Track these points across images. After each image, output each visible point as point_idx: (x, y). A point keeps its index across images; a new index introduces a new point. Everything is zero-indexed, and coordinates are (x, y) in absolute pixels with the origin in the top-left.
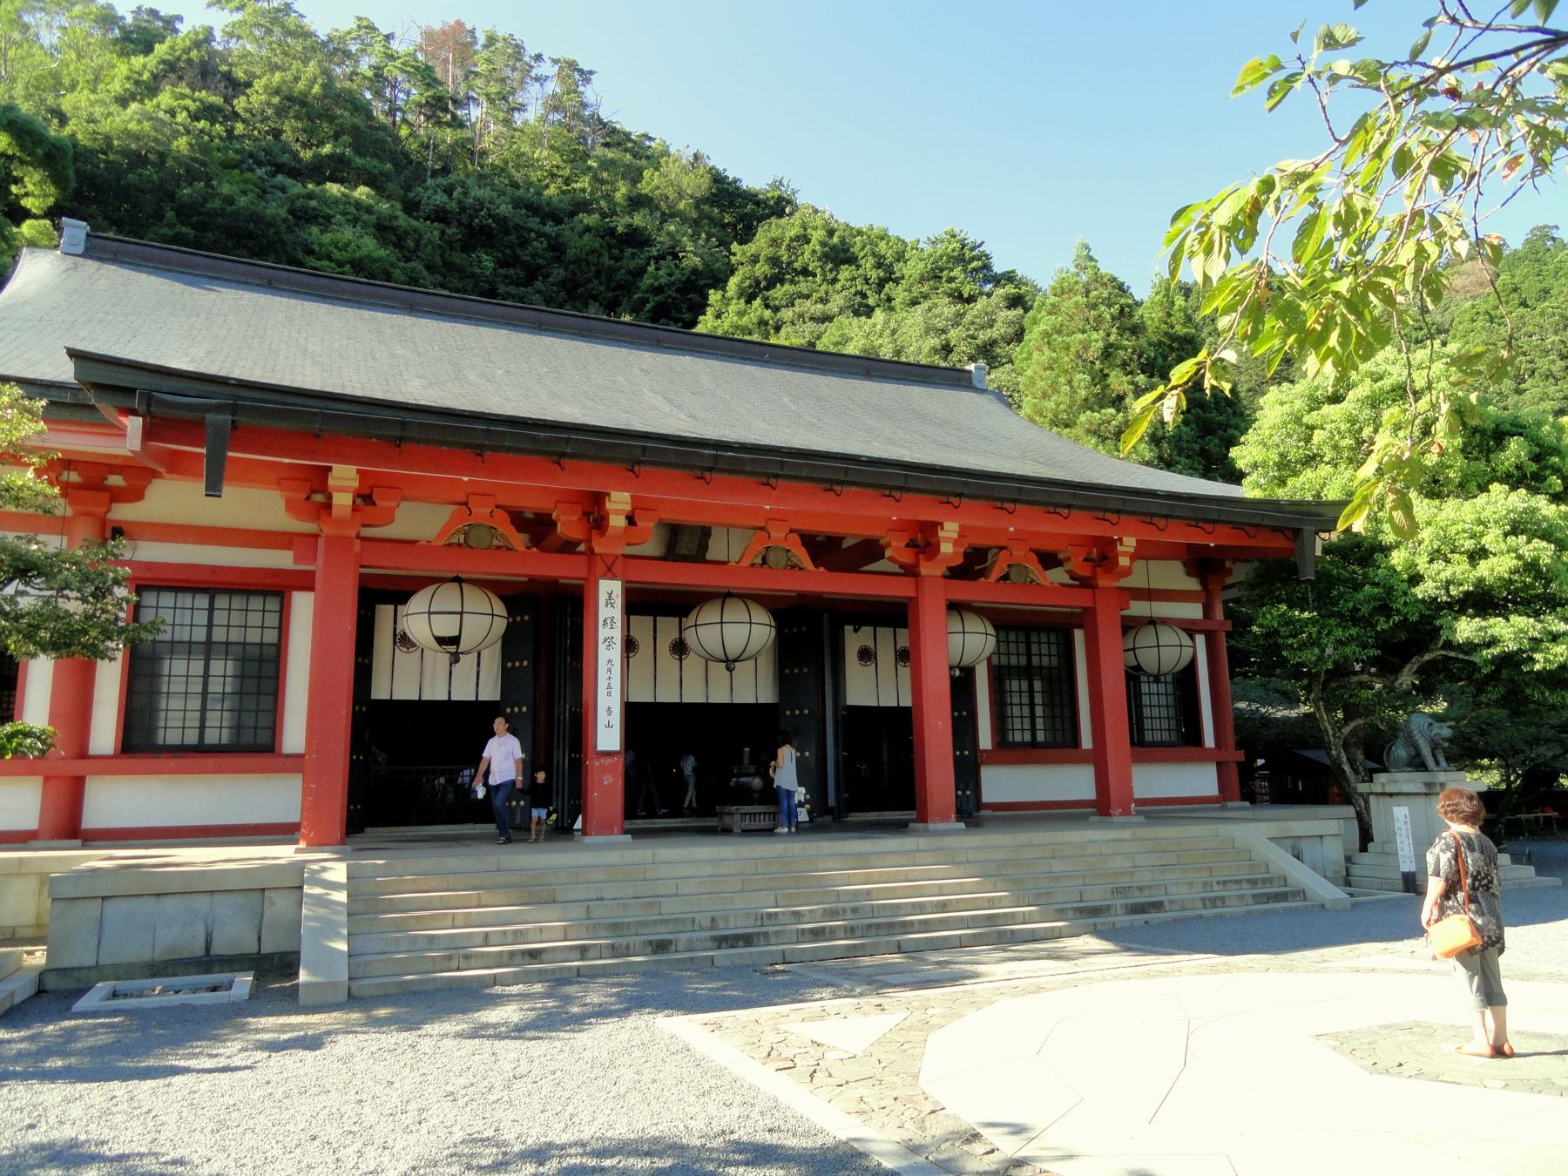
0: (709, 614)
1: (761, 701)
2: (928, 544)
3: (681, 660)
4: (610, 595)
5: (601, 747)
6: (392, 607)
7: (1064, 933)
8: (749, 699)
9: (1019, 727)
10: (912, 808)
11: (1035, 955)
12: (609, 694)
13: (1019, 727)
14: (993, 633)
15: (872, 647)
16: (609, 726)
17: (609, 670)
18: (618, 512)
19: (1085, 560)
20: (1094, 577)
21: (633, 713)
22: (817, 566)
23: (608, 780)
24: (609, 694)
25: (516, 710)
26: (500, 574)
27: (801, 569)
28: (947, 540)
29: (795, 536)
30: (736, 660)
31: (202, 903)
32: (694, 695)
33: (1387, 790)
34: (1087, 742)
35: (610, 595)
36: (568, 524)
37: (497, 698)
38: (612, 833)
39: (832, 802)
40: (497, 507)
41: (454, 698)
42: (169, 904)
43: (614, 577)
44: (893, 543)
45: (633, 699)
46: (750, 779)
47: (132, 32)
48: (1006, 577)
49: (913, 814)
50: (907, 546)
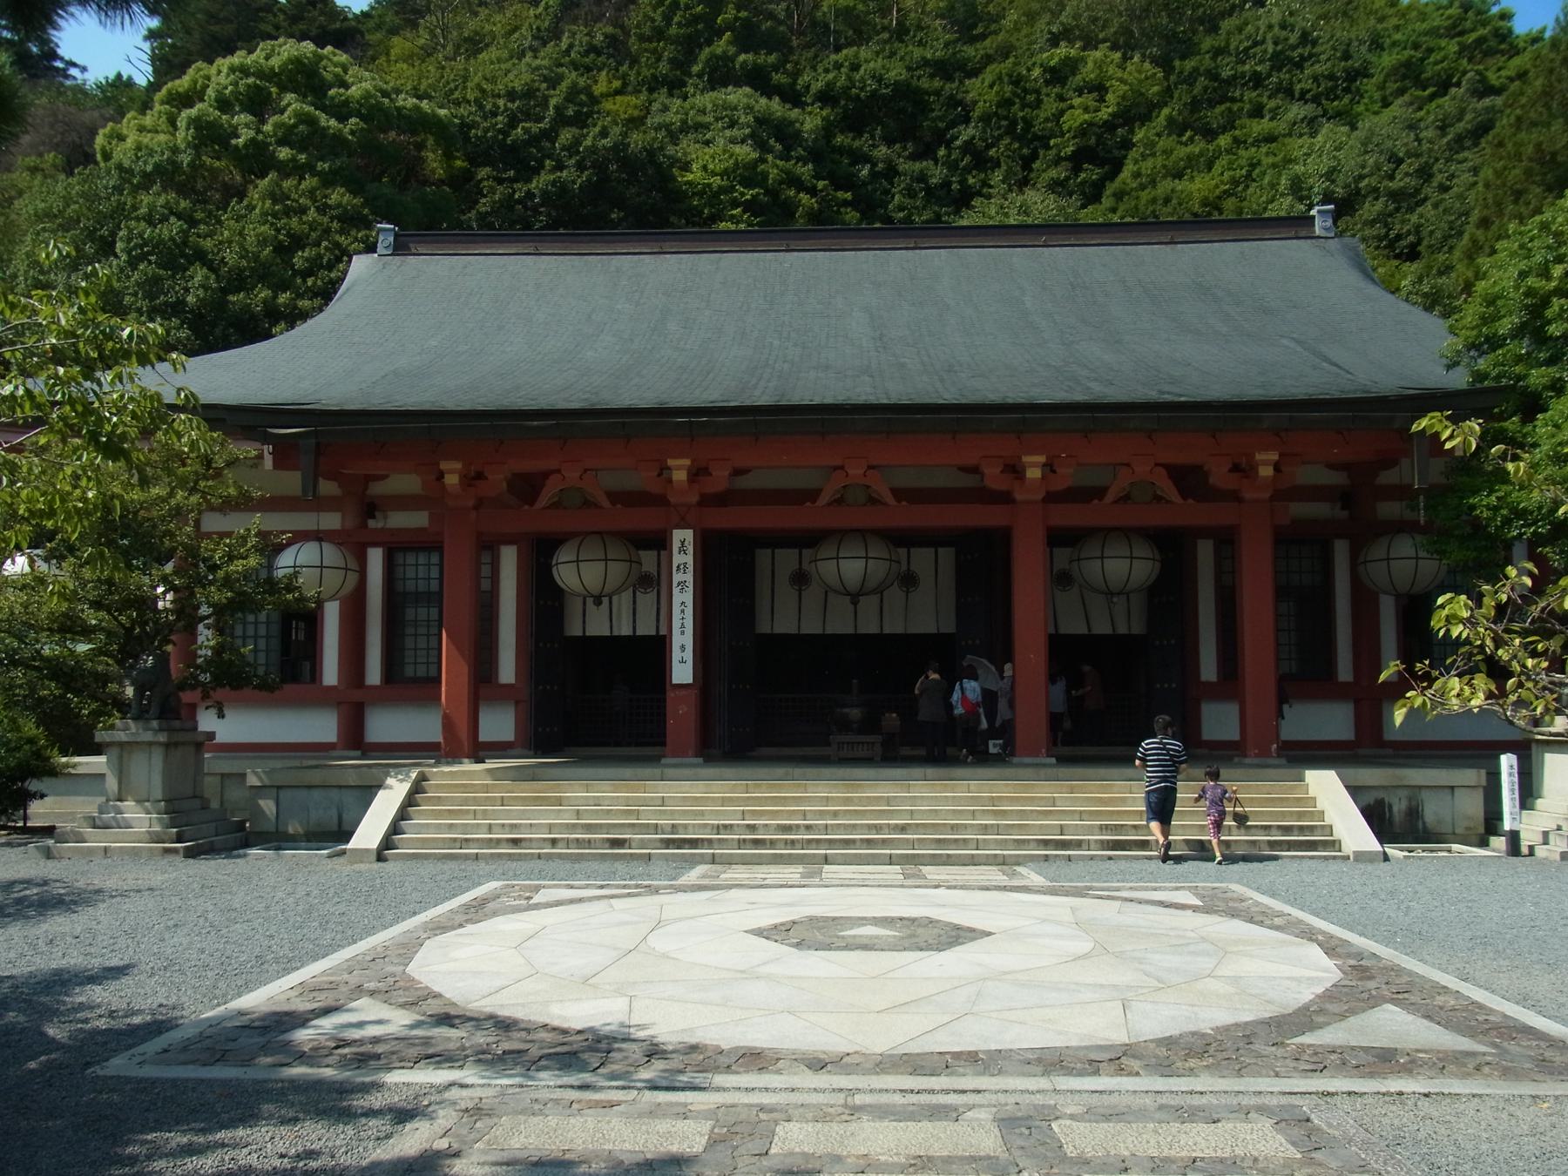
0: (827, 550)
4: (683, 543)
7: (1008, 861)
9: (425, 646)
11: (838, 882)
12: (683, 633)
13: (425, 646)
16: (682, 661)
17: (683, 611)
18: (1266, 463)
22: (1185, 498)
24: (683, 633)
29: (1163, 471)
31: (334, 794)
32: (811, 627)
34: (331, 673)
35: (683, 543)
36: (1219, 476)
38: (687, 756)
42: (316, 794)
47: (295, 126)
50: (1230, 471)
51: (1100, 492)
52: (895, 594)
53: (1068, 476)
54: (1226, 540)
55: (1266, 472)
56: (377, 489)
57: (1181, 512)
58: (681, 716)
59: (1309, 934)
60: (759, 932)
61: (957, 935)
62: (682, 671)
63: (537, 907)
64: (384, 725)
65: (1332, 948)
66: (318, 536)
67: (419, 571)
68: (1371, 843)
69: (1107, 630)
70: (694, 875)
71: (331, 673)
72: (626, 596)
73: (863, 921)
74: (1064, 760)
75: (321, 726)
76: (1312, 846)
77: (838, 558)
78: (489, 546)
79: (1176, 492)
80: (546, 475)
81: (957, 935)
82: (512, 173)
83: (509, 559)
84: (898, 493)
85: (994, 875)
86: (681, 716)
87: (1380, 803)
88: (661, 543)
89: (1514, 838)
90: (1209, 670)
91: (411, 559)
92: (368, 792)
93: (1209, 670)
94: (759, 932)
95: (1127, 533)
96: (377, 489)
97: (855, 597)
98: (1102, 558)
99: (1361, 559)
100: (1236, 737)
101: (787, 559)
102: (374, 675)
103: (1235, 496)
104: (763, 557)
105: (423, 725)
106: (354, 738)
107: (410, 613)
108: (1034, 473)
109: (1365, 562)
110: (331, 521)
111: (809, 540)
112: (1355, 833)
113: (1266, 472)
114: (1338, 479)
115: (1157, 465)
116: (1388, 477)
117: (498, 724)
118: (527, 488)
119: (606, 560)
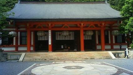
32: (61, 39)
34: (14, 44)
36: (99, 25)
51: (88, 27)
52: (69, 36)
53: (85, 25)
54: (99, 31)
55: (103, 25)
56: (19, 26)
57: (95, 28)
58: (50, 48)
59: (113, 66)
60: (63, 68)
61: (81, 68)
62: (50, 43)
63: (41, 66)
64: (20, 49)
65: (116, 67)
66: (13, 31)
67: (23, 34)
68: (115, 58)
70: (53, 62)
71: (14, 44)
72: (44, 37)
73: (72, 66)
75: (14, 49)
76: (109, 58)
78: (31, 31)
81: (81, 68)
82: (10, 33)
83: (32, 33)
84: (70, 27)
85: (81, 62)
86: (50, 48)
87: (115, 54)
88: (48, 32)
89: (128, 56)
90: (97, 43)
91: (22, 33)
92: (20, 55)
93: (97, 43)
94: (63, 68)
95: (90, 30)
96: (19, 26)
97: (65, 36)
100: (101, 48)
101: (59, 33)
102: (19, 44)
103: (100, 27)
104: (56, 33)
105: (25, 49)
106: (17, 50)
107: (23, 38)
108: (82, 25)
110: (14, 29)
111: (62, 31)
112: (113, 57)
113: (103, 25)
114: (109, 25)
116: (113, 25)
117: (32, 49)
118: (34, 26)
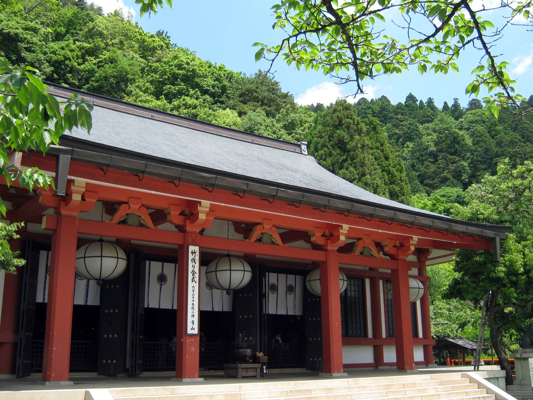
1: (216, 309)
2: (192, 214)
3: (161, 285)
5: (189, 331)
6: (276, 274)
8: (282, 312)
10: (174, 370)
14: (250, 269)
15: (276, 284)
18: (203, 212)
19: (322, 236)
20: (326, 245)
21: (203, 315)
23: (193, 349)
25: (112, 311)
26: (237, 252)
27: (146, 227)
28: (203, 212)
30: (96, 279)
33: (523, 357)
34: (370, 335)
37: (298, 312)
38: (194, 377)
39: (128, 365)
40: (274, 226)
41: (161, 308)
43: (195, 245)
44: (316, 234)
45: (201, 309)
46: (245, 350)
48: (259, 240)
49: (173, 373)
50: (180, 214)
69: (284, 313)
71: (370, 335)
74: (399, 371)
77: (102, 257)
79: (151, 221)
80: (121, 203)
95: (120, 243)
98: (231, 270)
99: (307, 279)
109: (310, 281)
115: (143, 205)
119: (244, 271)
